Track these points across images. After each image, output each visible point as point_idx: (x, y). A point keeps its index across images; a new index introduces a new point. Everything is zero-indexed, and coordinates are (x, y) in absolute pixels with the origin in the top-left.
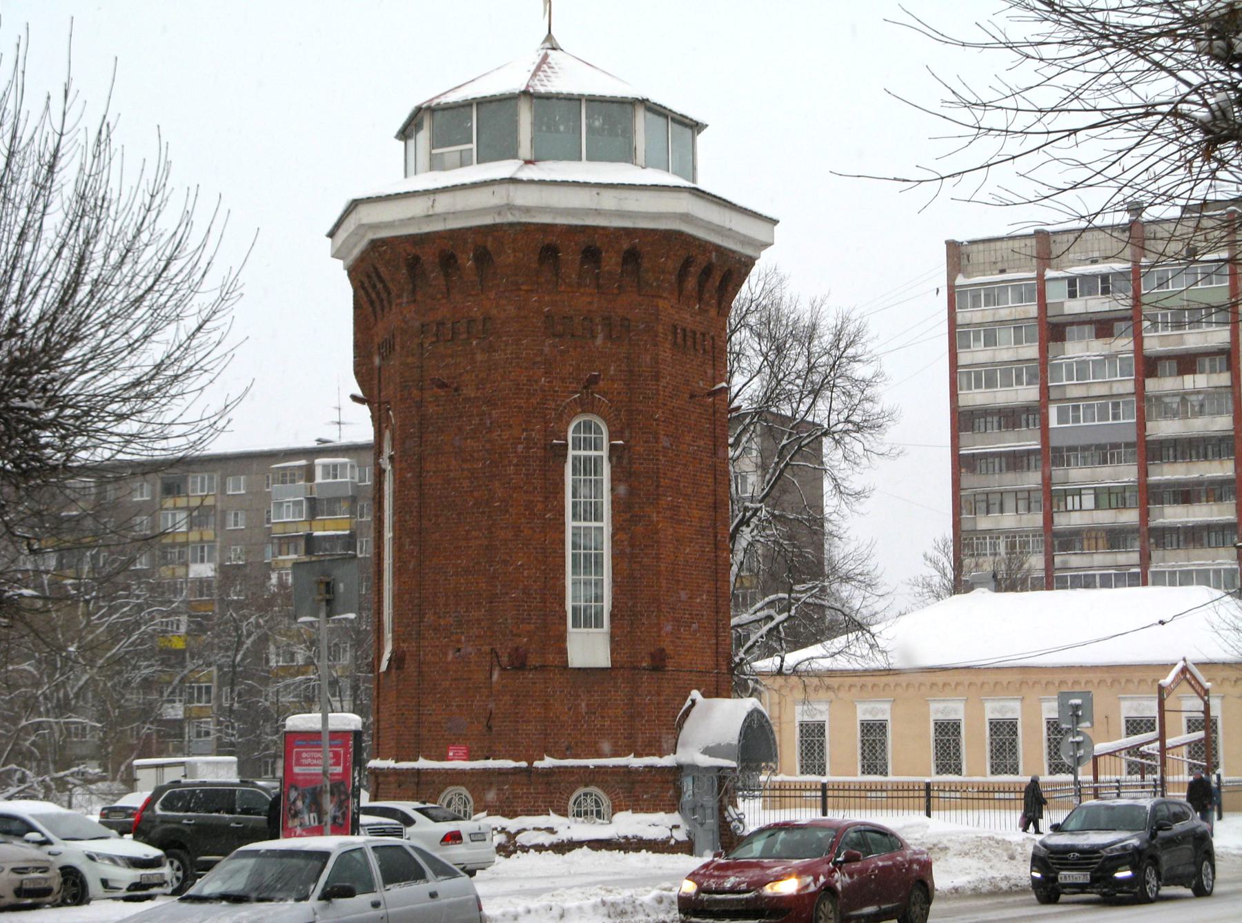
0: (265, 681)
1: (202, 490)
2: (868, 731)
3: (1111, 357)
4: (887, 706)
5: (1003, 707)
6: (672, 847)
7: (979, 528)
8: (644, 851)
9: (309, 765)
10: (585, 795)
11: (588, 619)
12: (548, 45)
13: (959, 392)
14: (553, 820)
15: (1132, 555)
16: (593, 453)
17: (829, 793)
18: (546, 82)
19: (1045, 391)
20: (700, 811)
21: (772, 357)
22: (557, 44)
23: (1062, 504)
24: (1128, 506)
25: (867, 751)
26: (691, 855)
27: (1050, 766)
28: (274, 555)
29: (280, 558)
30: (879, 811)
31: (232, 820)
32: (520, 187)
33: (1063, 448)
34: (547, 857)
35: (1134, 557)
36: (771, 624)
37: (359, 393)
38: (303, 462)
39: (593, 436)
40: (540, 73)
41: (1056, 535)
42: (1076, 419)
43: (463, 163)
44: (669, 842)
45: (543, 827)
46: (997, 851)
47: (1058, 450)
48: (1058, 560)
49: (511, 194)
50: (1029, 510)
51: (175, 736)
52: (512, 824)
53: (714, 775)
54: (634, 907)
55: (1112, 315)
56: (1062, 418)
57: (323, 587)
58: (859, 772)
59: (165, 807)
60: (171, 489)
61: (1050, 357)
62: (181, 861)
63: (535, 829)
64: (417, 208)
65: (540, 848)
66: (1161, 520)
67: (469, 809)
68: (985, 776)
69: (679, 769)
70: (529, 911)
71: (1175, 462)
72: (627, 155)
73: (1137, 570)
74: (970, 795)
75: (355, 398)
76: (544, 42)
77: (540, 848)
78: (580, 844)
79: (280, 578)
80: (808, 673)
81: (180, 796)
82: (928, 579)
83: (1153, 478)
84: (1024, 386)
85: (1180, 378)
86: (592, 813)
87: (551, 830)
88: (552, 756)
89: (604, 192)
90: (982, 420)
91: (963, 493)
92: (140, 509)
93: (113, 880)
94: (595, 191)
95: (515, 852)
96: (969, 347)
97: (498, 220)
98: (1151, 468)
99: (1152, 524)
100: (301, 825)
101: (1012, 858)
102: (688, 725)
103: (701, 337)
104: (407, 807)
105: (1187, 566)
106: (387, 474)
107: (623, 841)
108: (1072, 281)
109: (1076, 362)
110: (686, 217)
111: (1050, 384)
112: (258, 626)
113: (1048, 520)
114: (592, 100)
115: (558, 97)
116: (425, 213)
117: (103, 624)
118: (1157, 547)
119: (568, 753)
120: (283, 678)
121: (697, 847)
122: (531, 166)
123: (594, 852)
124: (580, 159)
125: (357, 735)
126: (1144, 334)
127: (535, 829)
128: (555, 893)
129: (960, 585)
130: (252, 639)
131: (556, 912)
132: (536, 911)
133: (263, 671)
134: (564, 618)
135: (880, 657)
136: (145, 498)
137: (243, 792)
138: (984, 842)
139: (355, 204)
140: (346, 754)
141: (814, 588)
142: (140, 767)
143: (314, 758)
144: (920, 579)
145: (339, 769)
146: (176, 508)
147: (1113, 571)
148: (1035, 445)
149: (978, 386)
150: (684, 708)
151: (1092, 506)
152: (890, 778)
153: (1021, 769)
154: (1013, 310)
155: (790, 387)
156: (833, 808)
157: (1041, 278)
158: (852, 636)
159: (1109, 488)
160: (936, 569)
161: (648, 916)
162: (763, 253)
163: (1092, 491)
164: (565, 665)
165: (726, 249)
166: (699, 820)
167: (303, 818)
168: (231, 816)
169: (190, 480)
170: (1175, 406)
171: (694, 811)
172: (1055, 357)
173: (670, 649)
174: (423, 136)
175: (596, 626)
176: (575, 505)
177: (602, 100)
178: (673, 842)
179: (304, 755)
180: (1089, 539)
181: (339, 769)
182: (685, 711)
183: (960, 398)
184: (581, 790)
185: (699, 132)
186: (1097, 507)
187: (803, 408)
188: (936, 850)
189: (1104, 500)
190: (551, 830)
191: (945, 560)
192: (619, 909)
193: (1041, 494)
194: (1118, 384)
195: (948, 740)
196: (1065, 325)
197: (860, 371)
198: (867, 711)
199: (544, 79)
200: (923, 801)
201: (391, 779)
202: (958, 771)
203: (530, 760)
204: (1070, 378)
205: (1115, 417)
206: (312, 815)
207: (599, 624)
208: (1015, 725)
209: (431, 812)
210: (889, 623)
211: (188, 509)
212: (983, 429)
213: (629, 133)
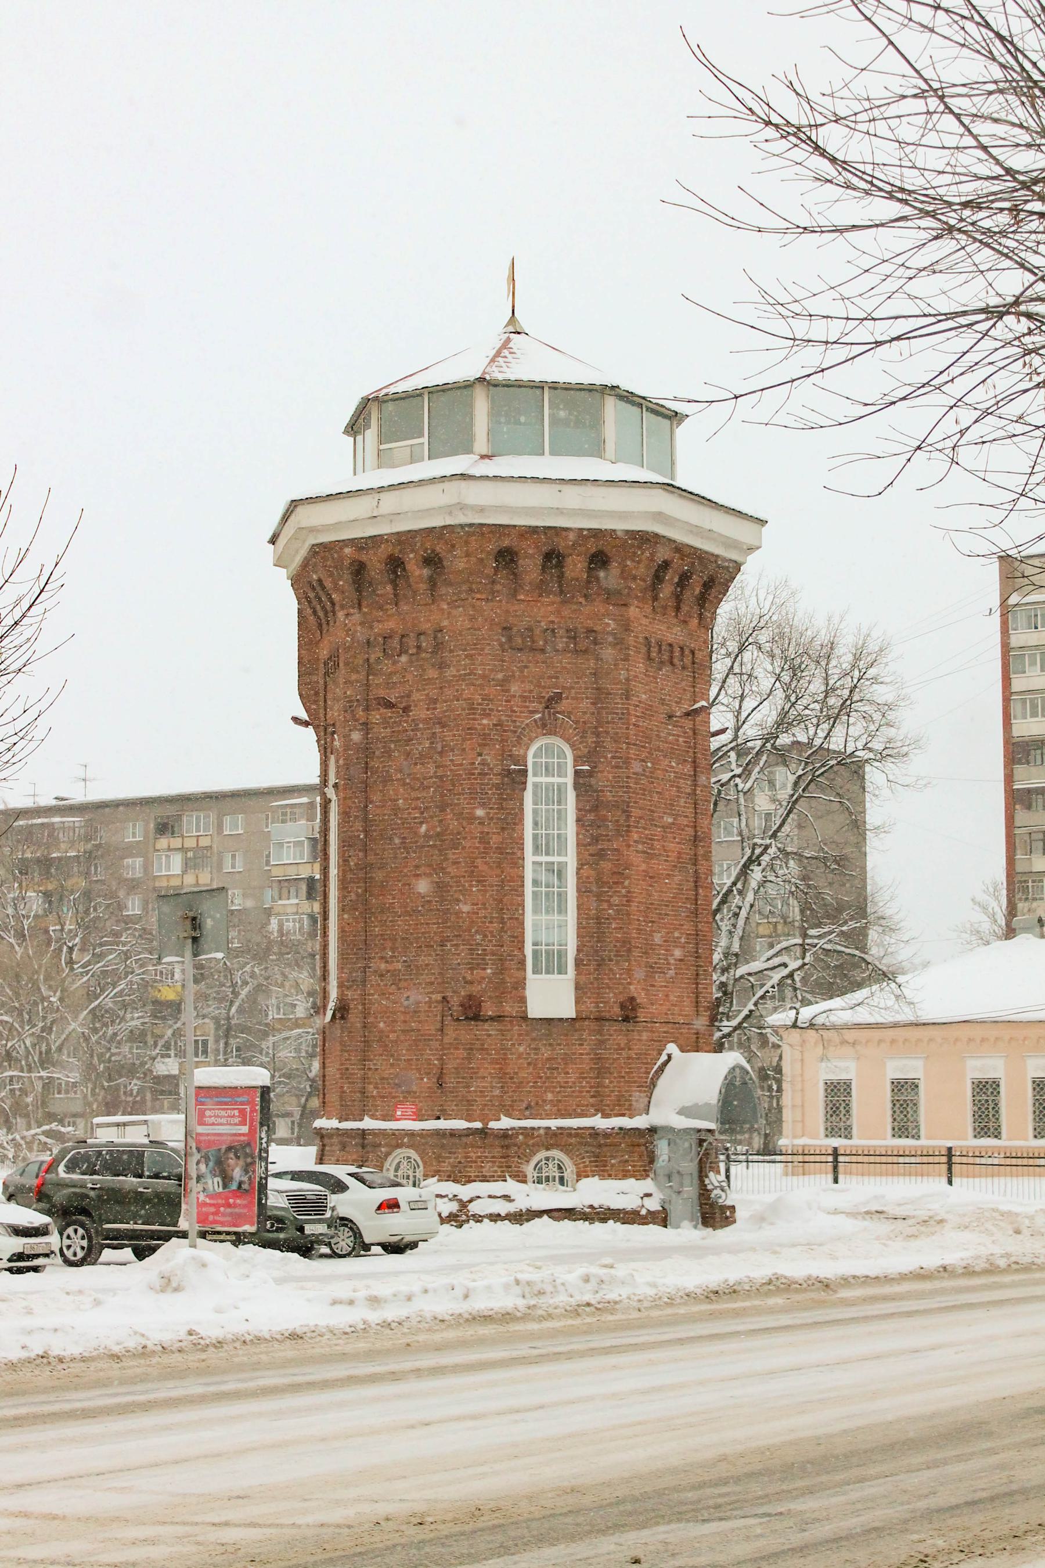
0: (265, 1035)
1: (198, 830)
2: (899, 1090)
4: (919, 1063)
6: (645, 1217)
7: (1034, 870)
8: (611, 1222)
9: (213, 1124)
10: (547, 1159)
11: (552, 963)
13: (1013, 721)
14: (510, 1186)
16: (556, 780)
17: (841, 1159)
18: (505, 369)
20: (676, 1178)
21: (786, 677)
25: (898, 1112)
26: (666, 1227)
28: (273, 900)
29: (280, 902)
30: (907, 1178)
31: (140, 1184)
32: (471, 484)
36: (785, 972)
37: (304, 715)
38: (305, 800)
39: (556, 760)
40: (499, 359)
43: (414, 459)
45: (499, 1195)
46: (1001, 1223)
51: (170, 1093)
52: (465, 1191)
53: (695, 1137)
54: (555, 1287)
57: (188, 923)
59: (69, 1169)
60: (164, 828)
62: (86, 1230)
63: (490, 1197)
64: (360, 508)
65: (495, 1218)
67: (420, 1173)
68: (1026, 1139)
69: (653, 1130)
70: (426, 1291)
72: (597, 450)
74: (996, 1161)
75: (296, 720)
77: (495, 1218)
78: (540, 1213)
79: (281, 925)
80: (824, 1027)
81: (86, 1158)
82: (976, 925)
87: (507, 1198)
88: (509, 1115)
89: (568, 489)
90: (1039, 752)
91: (1017, 831)
92: (130, 850)
95: (468, 1221)
96: (1024, 672)
100: (204, 1190)
101: (1018, 1232)
102: (661, 1082)
103: (668, 648)
104: (340, 1171)
106: (333, 802)
107: (588, 1210)
110: (659, 516)
112: (253, 975)
114: (554, 386)
115: (518, 385)
116: (370, 515)
117: (87, 973)
119: (527, 1113)
120: (279, 1031)
121: (673, 1217)
122: (487, 461)
123: (556, 1223)
125: (265, 1091)
127: (490, 1197)
128: (472, 1269)
129: (1010, 932)
130: (247, 990)
131: (459, 1292)
132: (435, 1291)
133: (259, 1023)
134: (522, 963)
135: (907, 1009)
136: (138, 839)
138: (987, 1214)
139: (294, 504)
140: (252, 1112)
141: (831, 933)
142: (99, 1126)
143: (218, 1116)
144: (968, 926)
145: (245, 1129)
146: (169, 849)
149: (1034, 714)
150: (656, 1067)
152: (923, 1142)
155: (807, 712)
156: (845, 1173)
158: (875, 987)
160: (985, 913)
161: (571, 1296)
162: (749, 558)
164: (525, 1018)
165: (706, 552)
166: (676, 1187)
167: (206, 1183)
168: (139, 1180)
169: (185, 818)
171: (669, 1177)
173: (641, 998)
174: (371, 434)
175: (560, 973)
176: (535, 837)
177: (568, 388)
178: (643, 1212)
179: (208, 1113)
181: (245, 1129)
183: (1014, 727)
184: (542, 1154)
185: (679, 424)
187: (821, 734)
188: (932, 1222)
190: (507, 1198)
191: (994, 904)
192: (536, 1289)
195: (987, 1101)
197: (882, 693)
198: (897, 1068)
199: (504, 365)
200: (945, 1167)
201: (335, 1140)
203: (485, 1120)
206: (216, 1180)
207: (562, 970)
208: (849, 1086)
209: (367, 1177)
210: (916, 973)
211: (183, 849)
212: (1039, 762)
213: (597, 422)
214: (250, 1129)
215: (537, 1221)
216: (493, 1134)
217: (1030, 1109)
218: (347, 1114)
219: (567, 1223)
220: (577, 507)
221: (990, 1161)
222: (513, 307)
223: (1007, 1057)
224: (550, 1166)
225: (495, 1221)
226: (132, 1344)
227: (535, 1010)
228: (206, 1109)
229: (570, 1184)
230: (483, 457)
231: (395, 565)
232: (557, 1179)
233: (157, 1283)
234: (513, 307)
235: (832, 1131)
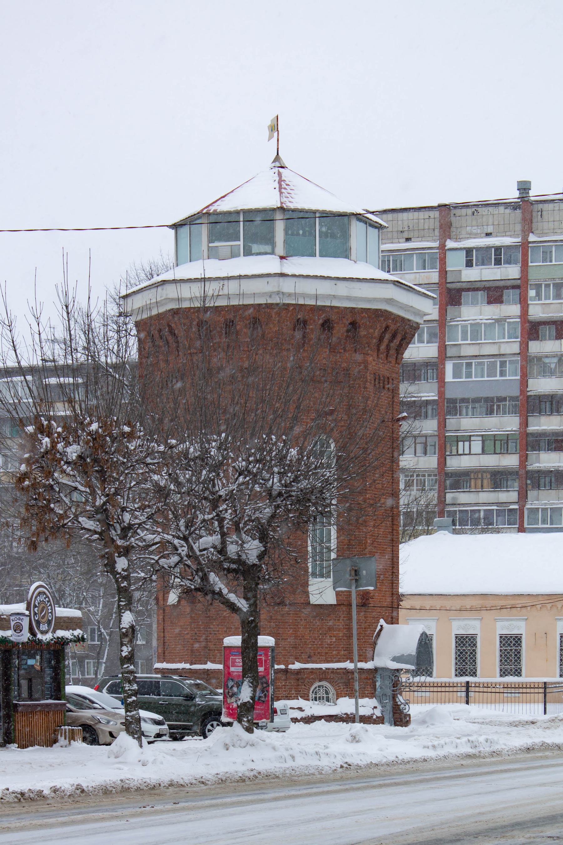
3: (500, 321)
5: (466, 625)
6: (375, 720)
10: (319, 687)
12: (277, 164)
14: (301, 702)
15: (511, 493)
19: (443, 349)
22: (284, 164)
23: (454, 448)
24: (509, 452)
27: (501, 670)
31: (160, 699)
33: (456, 399)
34: (300, 726)
35: (513, 496)
41: (448, 475)
42: (469, 375)
43: (234, 255)
44: (372, 717)
47: (453, 401)
48: (449, 497)
49: (281, 284)
50: (425, 453)
55: (501, 284)
56: (456, 374)
58: (498, 674)
61: (448, 318)
66: (537, 465)
69: (376, 670)
71: (551, 414)
72: (345, 253)
73: (516, 507)
74: (498, 690)
76: (274, 162)
78: (319, 718)
83: (532, 428)
84: (425, 344)
85: (558, 342)
86: (323, 699)
87: (300, 709)
89: (340, 283)
93: (147, 732)
94: (334, 282)
97: (270, 301)
98: (530, 419)
99: (530, 468)
102: (380, 642)
105: (557, 504)
108: (469, 251)
109: (471, 324)
110: (390, 301)
111: (447, 343)
113: (442, 462)
118: (533, 487)
124: (315, 255)
126: (529, 302)
137: (164, 683)
147: (495, 508)
148: (432, 396)
150: (376, 633)
151: (480, 451)
153: (478, 673)
154: (418, 275)
157: (442, 247)
159: (495, 435)
163: (480, 438)
164: (308, 603)
168: (158, 697)
170: (553, 366)
172: (452, 320)
178: (375, 717)
180: (476, 479)
182: (378, 633)
184: (317, 684)
186: (484, 452)
189: (490, 444)
190: (300, 709)
193: (436, 439)
194: (506, 345)
196: (460, 291)
202: (430, 675)
204: (464, 338)
205: (502, 374)
213: (346, 236)
214: (265, 669)
215: (317, 723)
216: (291, 672)
217: (453, 656)
218: (196, 660)
219: (333, 723)
220: (345, 295)
221: (493, 690)
222: (278, 149)
223: (438, 620)
224: (322, 690)
225: (295, 722)
226: (384, 760)
227: (314, 599)
228: (236, 659)
229: (332, 701)
230: (282, 258)
231: (229, 324)
232: (325, 698)
233: (350, 738)
234: (278, 149)
235: (461, 672)
